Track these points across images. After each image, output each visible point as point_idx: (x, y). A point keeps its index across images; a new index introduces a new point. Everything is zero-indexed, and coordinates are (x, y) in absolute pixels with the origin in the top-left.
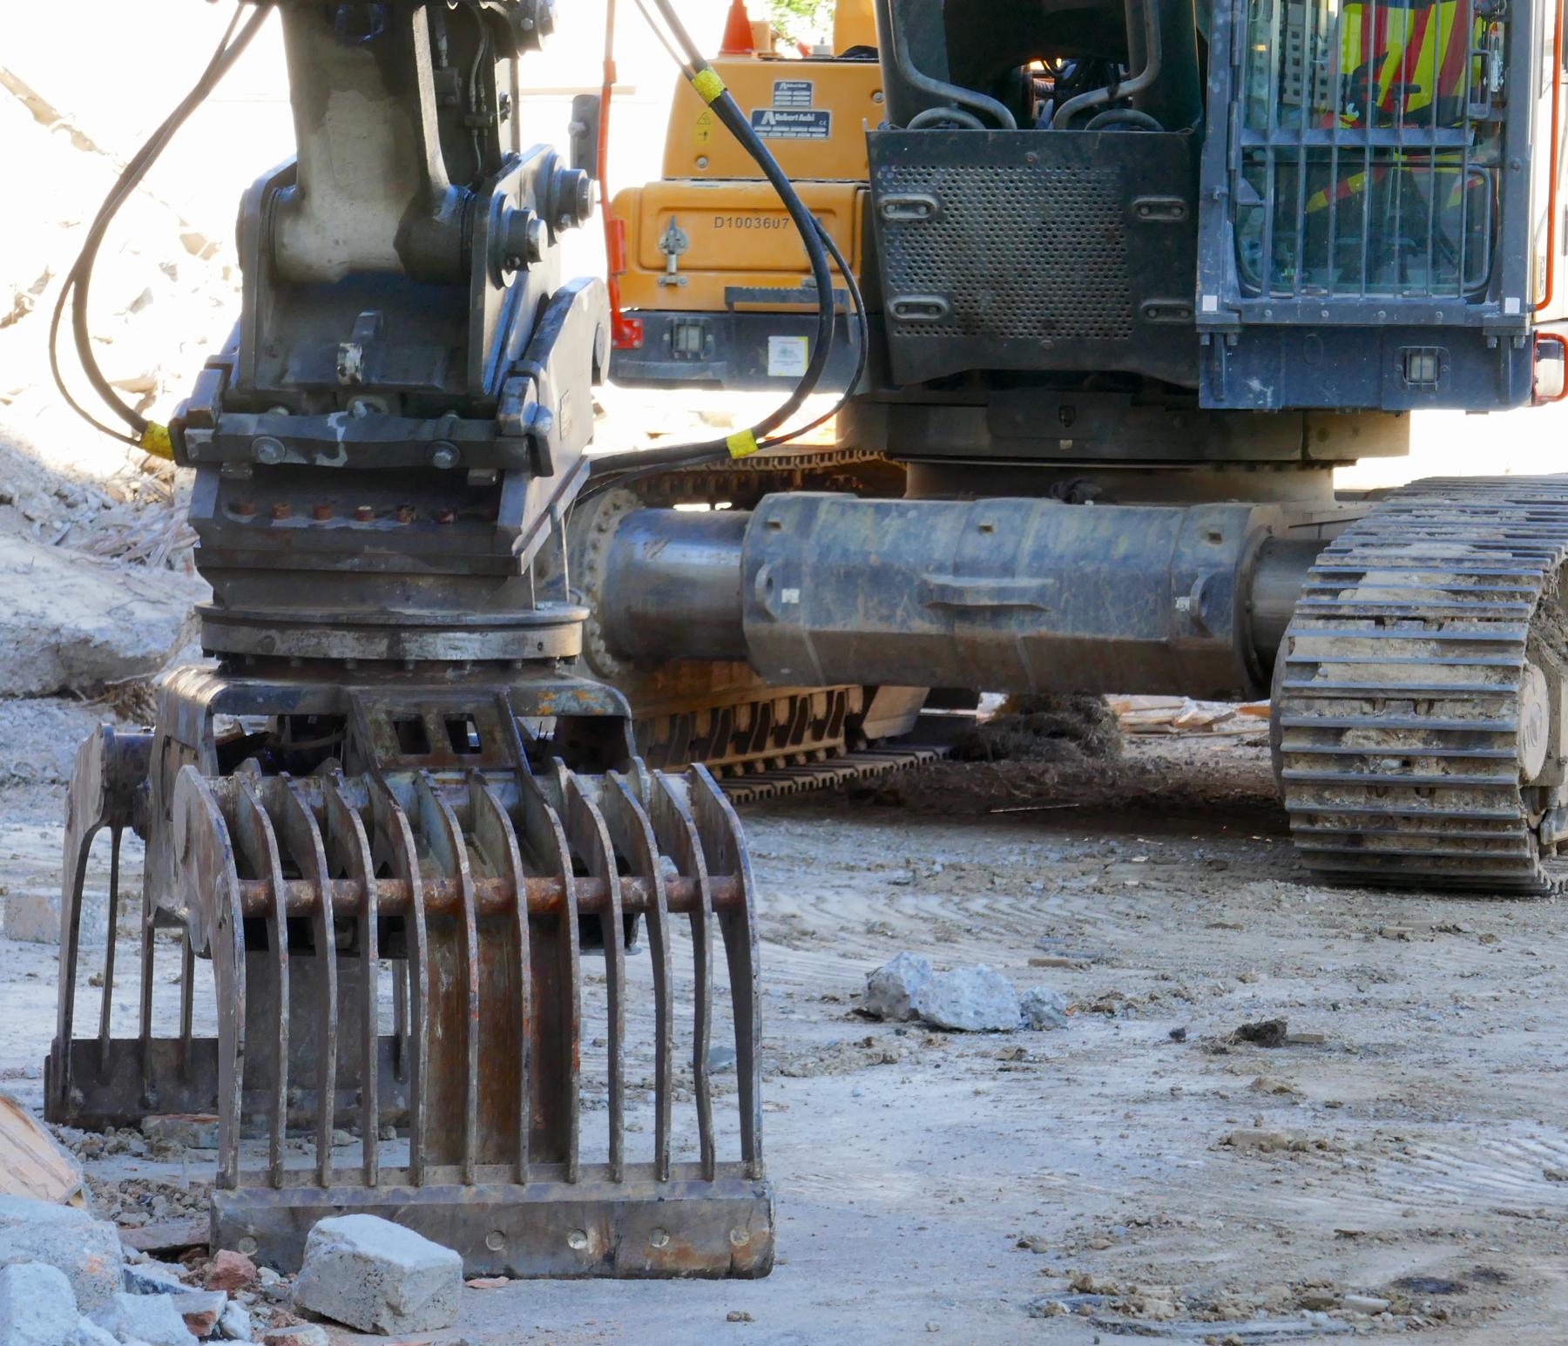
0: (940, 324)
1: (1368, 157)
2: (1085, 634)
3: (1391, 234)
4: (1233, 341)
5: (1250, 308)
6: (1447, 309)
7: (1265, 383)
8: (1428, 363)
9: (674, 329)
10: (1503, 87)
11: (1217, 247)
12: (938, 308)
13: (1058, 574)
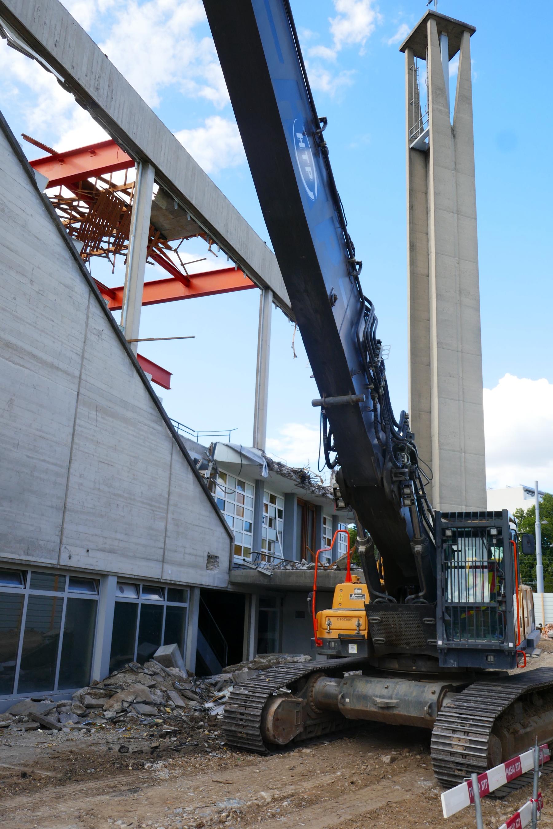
0: (384, 644)
1: (466, 609)
2: (406, 714)
3: (481, 626)
4: (445, 651)
5: (449, 644)
6: (495, 646)
7: (454, 661)
8: (492, 657)
9: (330, 642)
10: (504, 593)
11: (440, 629)
12: (383, 641)
13: (401, 700)
